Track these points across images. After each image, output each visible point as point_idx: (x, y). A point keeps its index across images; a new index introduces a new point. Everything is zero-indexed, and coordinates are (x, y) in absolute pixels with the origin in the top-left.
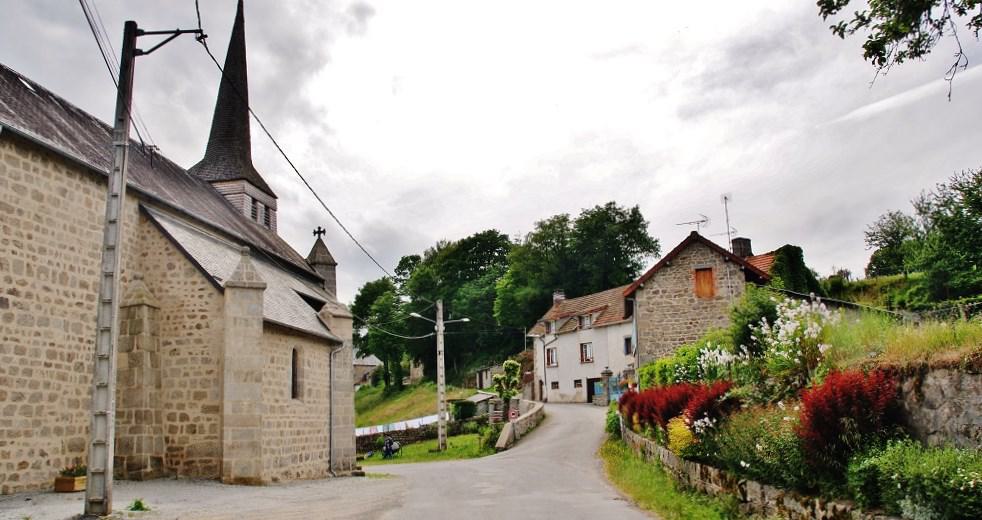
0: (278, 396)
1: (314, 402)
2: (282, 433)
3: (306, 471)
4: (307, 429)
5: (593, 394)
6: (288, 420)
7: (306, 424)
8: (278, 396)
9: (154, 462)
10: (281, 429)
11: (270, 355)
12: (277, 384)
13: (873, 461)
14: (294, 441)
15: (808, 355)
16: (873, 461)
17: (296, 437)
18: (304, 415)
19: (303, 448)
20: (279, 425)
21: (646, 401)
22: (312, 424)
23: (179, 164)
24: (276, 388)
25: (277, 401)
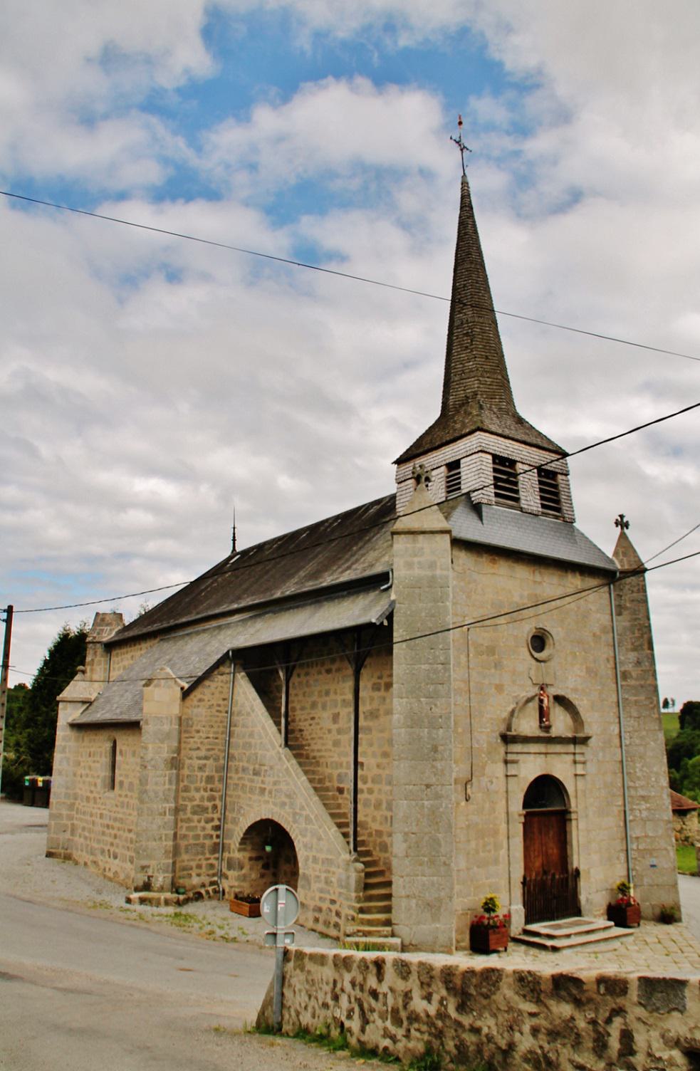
0: (93, 788)
1: (126, 796)
2: (93, 823)
3: (113, 870)
4: (117, 824)
5: (528, 698)
6: (99, 812)
7: (115, 819)
8: (93, 788)
9: (676, 916)
10: (94, 818)
11: (88, 750)
12: (93, 776)
13: (408, 572)
14: (103, 833)
15: (340, 1055)
16: (408, 572)
17: (105, 829)
18: (115, 809)
19: (112, 844)
20: (91, 816)
21: (670, 826)
22: (121, 820)
23: (220, 561)
24: (91, 780)
25: (92, 792)
